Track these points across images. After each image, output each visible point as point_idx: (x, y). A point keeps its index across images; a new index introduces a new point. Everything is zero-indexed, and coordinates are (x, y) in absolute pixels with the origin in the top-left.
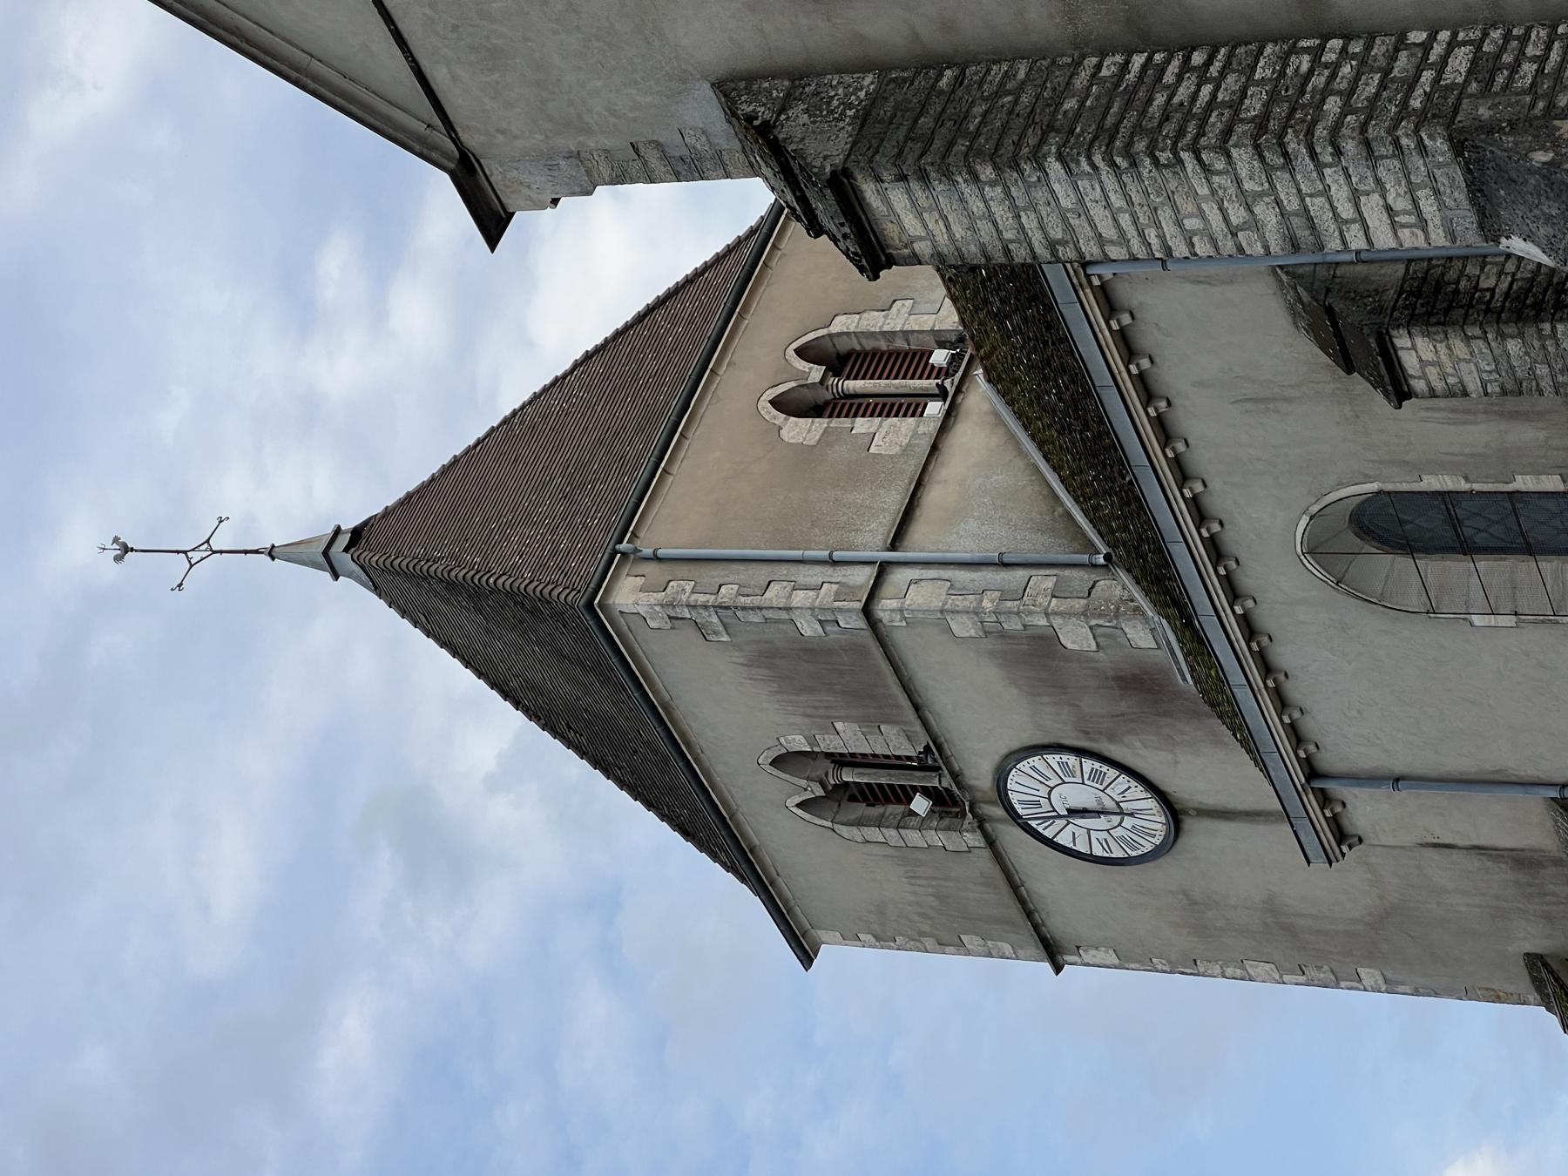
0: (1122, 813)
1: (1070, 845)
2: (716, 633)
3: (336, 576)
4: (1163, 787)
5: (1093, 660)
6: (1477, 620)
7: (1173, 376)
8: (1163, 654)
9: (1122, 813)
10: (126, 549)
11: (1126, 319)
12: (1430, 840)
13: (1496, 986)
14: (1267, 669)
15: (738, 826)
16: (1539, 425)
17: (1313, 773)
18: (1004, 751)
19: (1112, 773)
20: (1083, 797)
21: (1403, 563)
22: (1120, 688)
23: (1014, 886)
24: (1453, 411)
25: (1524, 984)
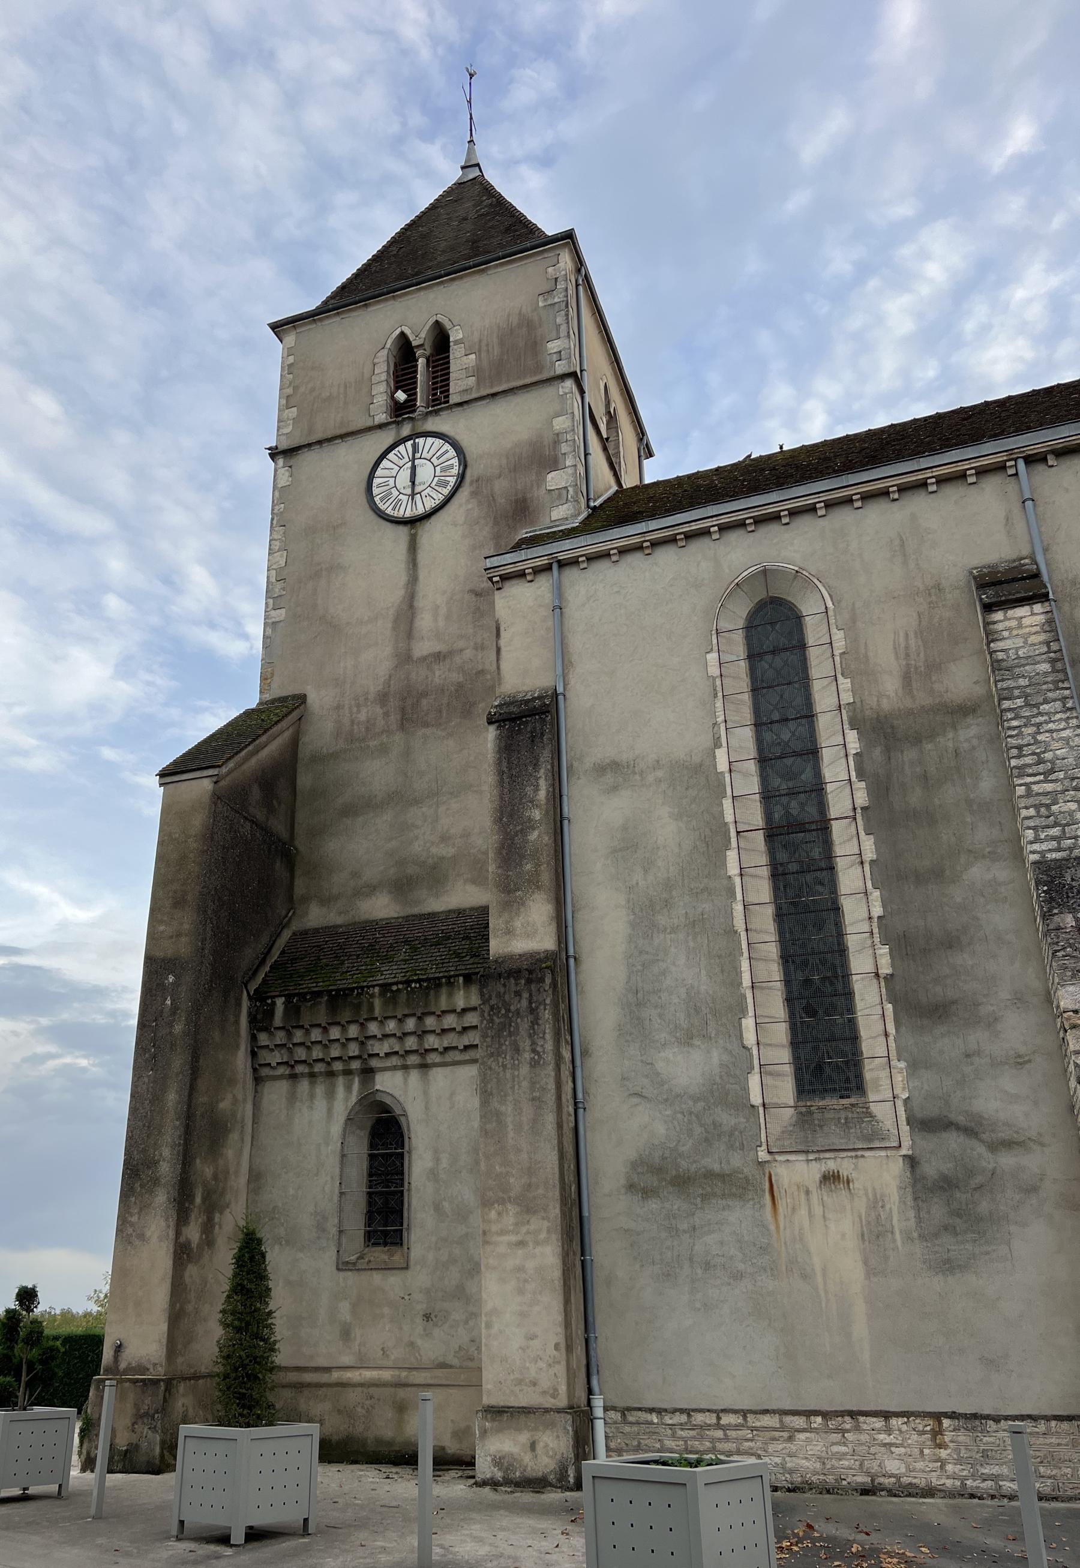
0: (413, 495)
1: (381, 466)
2: (545, 300)
3: (463, 168)
4: (434, 518)
5: (539, 487)
6: (712, 657)
7: (917, 503)
8: (547, 523)
9: (413, 495)
10: (471, 76)
11: (785, 520)
12: (502, 629)
13: (275, 678)
14: (655, 544)
15: (386, 300)
16: (900, 691)
17: (562, 564)
18: (458, 438)
19: (446, 491)
20: (425, 472)
21: (741, 623)
22: (516, 501)
23: (342, 437)
24: (907, 648)
25: (277, 692)
